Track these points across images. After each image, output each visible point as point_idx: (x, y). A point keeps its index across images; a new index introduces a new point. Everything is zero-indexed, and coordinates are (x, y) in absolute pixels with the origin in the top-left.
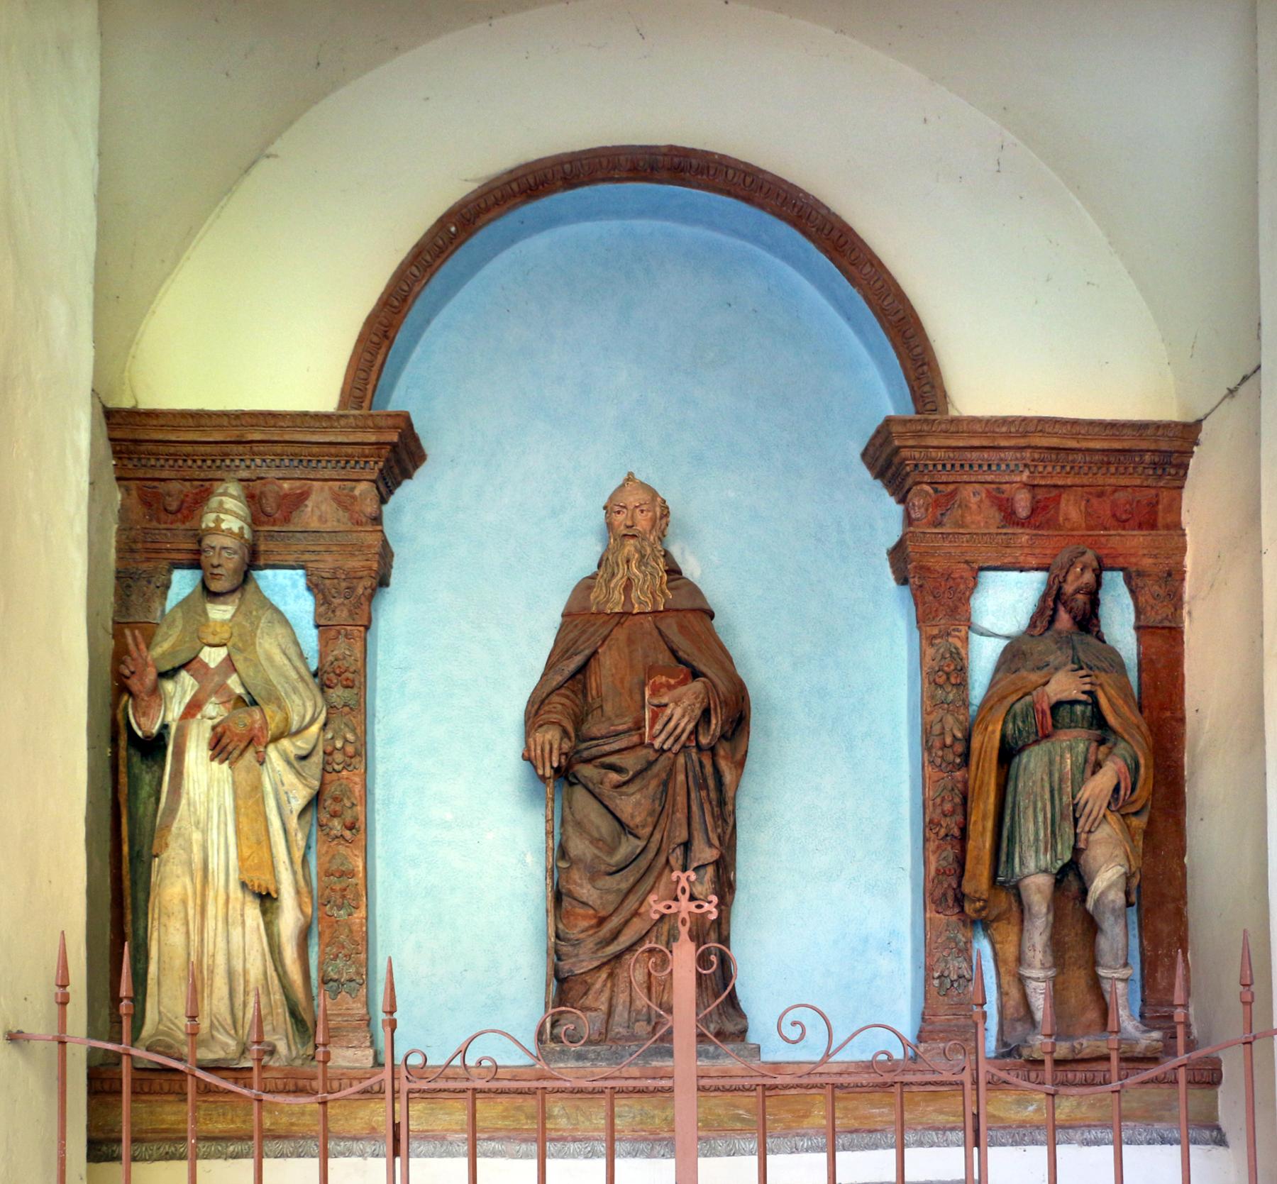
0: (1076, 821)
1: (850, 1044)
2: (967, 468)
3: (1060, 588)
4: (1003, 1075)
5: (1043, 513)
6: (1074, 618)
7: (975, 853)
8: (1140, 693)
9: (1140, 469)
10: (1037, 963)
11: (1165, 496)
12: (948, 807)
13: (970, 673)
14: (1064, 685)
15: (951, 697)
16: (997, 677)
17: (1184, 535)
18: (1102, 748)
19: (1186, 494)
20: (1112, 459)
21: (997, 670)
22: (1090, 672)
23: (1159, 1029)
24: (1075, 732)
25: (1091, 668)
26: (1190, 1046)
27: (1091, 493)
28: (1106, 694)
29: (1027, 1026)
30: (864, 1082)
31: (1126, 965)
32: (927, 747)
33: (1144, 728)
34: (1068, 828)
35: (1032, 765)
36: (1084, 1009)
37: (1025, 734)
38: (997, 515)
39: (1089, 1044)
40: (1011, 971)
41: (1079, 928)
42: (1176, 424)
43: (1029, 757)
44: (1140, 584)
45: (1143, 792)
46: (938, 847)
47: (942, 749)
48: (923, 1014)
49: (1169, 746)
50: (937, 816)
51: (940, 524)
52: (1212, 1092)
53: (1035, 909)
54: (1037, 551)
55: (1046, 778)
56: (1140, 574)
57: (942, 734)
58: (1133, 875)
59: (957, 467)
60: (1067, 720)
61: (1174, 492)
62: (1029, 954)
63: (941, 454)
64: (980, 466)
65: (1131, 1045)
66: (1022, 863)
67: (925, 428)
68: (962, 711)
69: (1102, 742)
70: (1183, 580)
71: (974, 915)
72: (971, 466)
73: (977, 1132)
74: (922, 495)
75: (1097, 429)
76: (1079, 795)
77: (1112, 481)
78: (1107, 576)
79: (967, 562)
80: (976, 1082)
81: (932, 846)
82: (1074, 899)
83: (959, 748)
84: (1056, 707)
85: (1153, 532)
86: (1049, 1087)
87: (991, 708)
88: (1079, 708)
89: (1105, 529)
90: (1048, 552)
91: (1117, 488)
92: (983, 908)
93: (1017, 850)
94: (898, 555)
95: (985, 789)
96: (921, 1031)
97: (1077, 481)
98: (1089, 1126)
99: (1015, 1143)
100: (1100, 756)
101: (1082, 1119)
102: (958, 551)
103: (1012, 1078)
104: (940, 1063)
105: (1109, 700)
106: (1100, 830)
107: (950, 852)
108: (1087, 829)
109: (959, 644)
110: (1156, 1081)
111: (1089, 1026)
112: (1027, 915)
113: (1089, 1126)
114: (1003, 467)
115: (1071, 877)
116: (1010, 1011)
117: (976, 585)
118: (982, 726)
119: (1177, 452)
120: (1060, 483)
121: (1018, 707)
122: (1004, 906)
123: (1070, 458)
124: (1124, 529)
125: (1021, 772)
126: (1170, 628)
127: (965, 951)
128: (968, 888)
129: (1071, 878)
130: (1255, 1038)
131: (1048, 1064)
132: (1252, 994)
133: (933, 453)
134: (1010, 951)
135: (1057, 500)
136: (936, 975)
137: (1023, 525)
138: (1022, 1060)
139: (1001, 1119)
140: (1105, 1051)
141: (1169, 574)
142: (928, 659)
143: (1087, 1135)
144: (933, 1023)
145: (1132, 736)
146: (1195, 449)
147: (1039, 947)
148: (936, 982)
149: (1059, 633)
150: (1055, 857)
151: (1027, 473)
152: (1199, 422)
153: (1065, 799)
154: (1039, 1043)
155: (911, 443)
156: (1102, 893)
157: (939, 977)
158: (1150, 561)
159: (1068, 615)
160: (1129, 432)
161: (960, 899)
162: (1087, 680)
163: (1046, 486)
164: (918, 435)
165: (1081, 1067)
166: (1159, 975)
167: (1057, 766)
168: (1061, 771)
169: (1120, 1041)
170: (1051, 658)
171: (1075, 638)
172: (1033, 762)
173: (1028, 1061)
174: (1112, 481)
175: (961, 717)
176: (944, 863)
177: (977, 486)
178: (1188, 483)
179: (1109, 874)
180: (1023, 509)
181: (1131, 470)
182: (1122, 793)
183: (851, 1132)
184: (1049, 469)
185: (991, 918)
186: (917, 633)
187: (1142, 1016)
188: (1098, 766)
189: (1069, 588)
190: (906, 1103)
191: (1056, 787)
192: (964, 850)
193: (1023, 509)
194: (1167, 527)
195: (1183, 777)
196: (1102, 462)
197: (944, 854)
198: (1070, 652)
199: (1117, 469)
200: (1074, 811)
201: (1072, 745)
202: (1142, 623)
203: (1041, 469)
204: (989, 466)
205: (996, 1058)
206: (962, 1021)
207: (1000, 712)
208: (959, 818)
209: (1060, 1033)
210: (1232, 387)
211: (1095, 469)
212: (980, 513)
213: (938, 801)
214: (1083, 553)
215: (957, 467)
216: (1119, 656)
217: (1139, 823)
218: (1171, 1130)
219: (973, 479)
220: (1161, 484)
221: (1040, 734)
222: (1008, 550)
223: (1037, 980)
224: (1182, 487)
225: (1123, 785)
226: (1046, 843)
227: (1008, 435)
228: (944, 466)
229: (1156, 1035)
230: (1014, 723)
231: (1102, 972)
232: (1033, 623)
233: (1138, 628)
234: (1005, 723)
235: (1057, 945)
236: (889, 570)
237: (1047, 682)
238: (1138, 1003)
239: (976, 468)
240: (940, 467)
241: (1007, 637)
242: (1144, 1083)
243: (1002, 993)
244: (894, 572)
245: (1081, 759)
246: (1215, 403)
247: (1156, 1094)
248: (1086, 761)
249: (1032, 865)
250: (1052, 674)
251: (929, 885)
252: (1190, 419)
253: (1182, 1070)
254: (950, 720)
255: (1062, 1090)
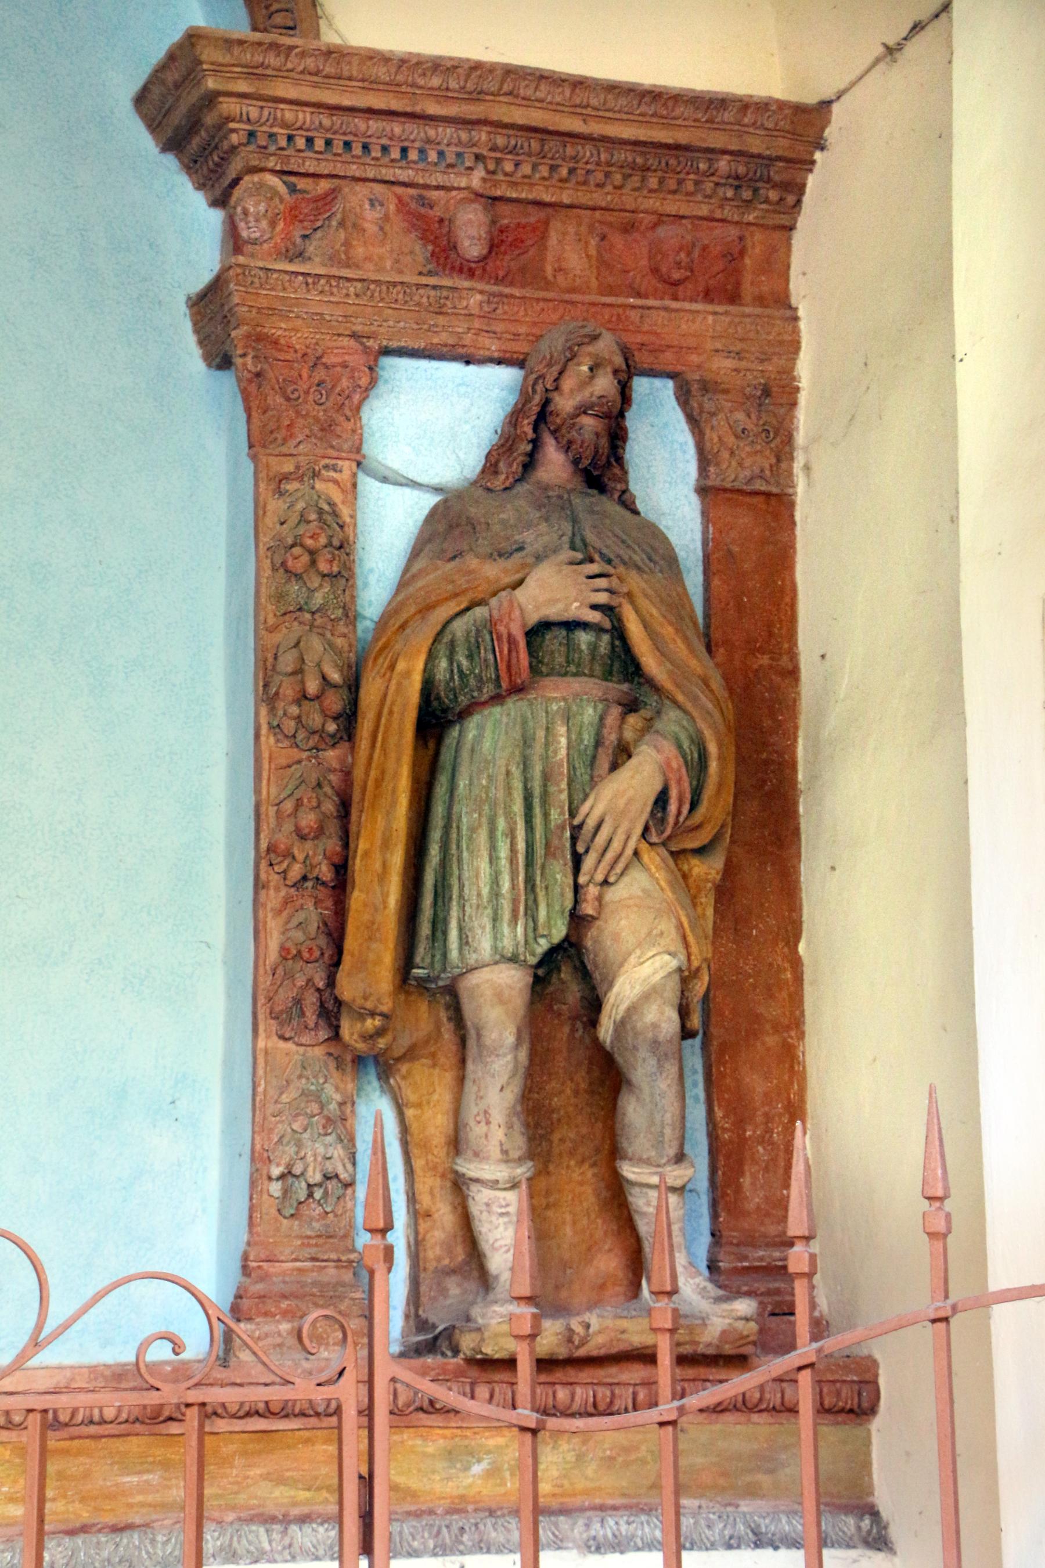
0: (577, 861)
1: (78, 1326)
2: (357, 150)
3: (546, 402)
4: (429, 1388)
5: (511, 251)
6: (576, 462)
7: (366, 917)
8: (707, 616)
9: (708, 186)
10: (495, 1152)
11: (757, 243)
12: (308, 819)
13: (359, 554)
14: (555, 590)
15: (318, 599)
16: (414, 569)
17: (796, 319)
18: (632, 719)
19: (799, 240)
20: (653, 162)
21: (416, 553)
22: (609, 569)
23: (749, 1294)
24: (577, 684)
25: (609, 562)
26: (819, 1328)
27: (610, 225)
28: (637, 611)
29: (472, 1285)
30: (109, 1413)
31: (680, 1158)
32: (267, 695)
33: (717, 682)
34: (560, 874)
35: (487, 744)
36: (590, 1251)
37: (472, 682)
38: (418, 247)
39: (602, 1326)
40: (446, 1159)
41: (582, 1080)
42: (782, 105)
43: (481, 728)
44: (709, 406)
45: (715, 807)
46: (286, 902)
47: (298, 702)
48: (245, 1258)
49: (767, 723)
50: (284, 837)
51: (300, 255)
52: (859, 1431)
53: (491, 1036)
54: (499, 327)
55: (516, 772)
56: (707, 387)
57: (299, 672)
58: (695, 974)
59: (338, 147)
60: (560, 659)
61: (778, 235)
62: (476, 1131)
63: (305, 116)
64: (385, 149)
65: (691, 1329)
66: (464, 941)
67: (272, 60)
68: (342, 628)
69: (631, 706)
70: (794, 404)
71: (361, 1046)
72: (366, 147)
73: (367, 1518)
74: (260, 199)
75: (623, 101)
76: (584, 809)
77: (652, 203)
78: (641, 385)
79: (354, 336)
80: (368, 1412)
81: (273, 898)
82: (574, 1018)
83: (335, 702)
84: (538, 631)
85: (731, 308)
86: (527, 1416)
87: (403, 627)
88: (584, 638)
89: (639, 295)
90: (523, 330)
91: (661, 219)
92: (380, 1032)
93: (454, 913)
94: (211, 310)
95: (387, 786)
96: (238, 1297)
97: (583, 198)
98: (602, 1508)
99: (442, 1550)
100: (629, 735)
101: (586, 1492)
102: (339, 311)
103: (449, 1396)
104: (288, 1362)
105: (646, 626)
106: (626, 879)
107: (312, 914)
108: (599, 877)
109: (337, 496)
110: (743, 1406)
111: (602, 1287)
112: (471, 1043)
113: (602, 1508)
114: (433, 156)
115: (566, 973)
116: (433, 1253)
117: (373, 382)
118: (384, 662)
119: (779, 158)
120: (547, 198)
121: (459, 627)
122: (425, 1026)
123: (569, 151)
124: (675, 298)
125: (465, 754)
126: (768, 495)
127: (339, 1124)
128: (348, 988)
129: (566, 973)
130: (954, 1309)
131: (525, 1367)
132: (948, 1216)
133: (289, 114)
134: (435, 1123)
135: (541, 231)
136: (276, 1171)
137: (471, 273)
138: (459, 1360)
139: (414, 1495)
140: (648, 1339)
141: (767, 392)
142: (270, 520)
143: (596, 1529)
144: (264, 1278)
145: (695, 699)
146: (818, 156)
147: (498, 1116)
148: (276, 1188)
149: (546, 488)
150: (534, 931)
151: (479, 173)
152: (826, 105)
153: (554, 814)
154: (500, 1323)
155: (242, 87)
156: (633, 1010)
157: (282, 1177)
158: (729, 363)
159: (564, 454)
160: (687, 111)
161: (331, 1011)
162: (602, 583)
163: (517, 201)
164: (254, 73)
165: (586, 1375)
166: (746, 1181)
167: (538, 748)
168: (545, 758)
169: (676, 1313)
170: (528, 536)
171: (577, 500)
172: (487, 739)
173: (470, 1361)
174: (652, 203)
175: (339, 642)
176: (299, 936)
177: (378, 188)
178: (802, 222)
179: (647, 969)
180: (471, 232)
181: (690, 186)
182: (673, 808)
183: (72, 1533)
184: (526, 169)
185: (397, 1052)
186: (248, 467)
187: (713, 1267)
188: (623, 753)
189: (565, 403)
190: (209, 1458)
191: (537, 791)
192: (341, 911)
193: (471, 232)
194: (760, 300)
195: (793, 783)
196: (633, 166)
197: (301, 916)
198: (567, 527)
199: (661, 181)
200: (574, 839)
201: (569, 710)
202: (714, 481)
203: (509, 167)
204: (404, 151)
205: (402, 1355)
206: (331, 1272)
207: (422, 636)
208: (332, 844)
209: (545, 1300)
210: (891, 43)
211: (618, 178)
212: (382, 243)
213: (288, 806)
214: (595, 338)
215: (338, 147)
216: (665, 540)
217: (707, 870)
218: (774, 1515)
219: (371, 174)
220: (751, 218)
221: (505, 685)
222: (441, 320)
223: (494, 1184)
224: (791, 228)
225: (674, 793)
226: (515, 902)
227: (443, 95)
228: (310, 141)
229: (745, 1306)
230: (451, 660)
231: (629, 1171)
232: (491, 466)
233: (702, 491)
234: (431, 656)
235: (536, 1117)
236: (190, 340)
237: (520, 583)
238: (706, 1239)
239: (376, 153)
240: (301, 143)
241: (437, 489)
242: (718, 1409)
243: (417, 1214)
244: (201, 343)
245: (588, 739)
246: (858, 72)
247: (743, 1435)
248: (598, 743)
249: (484, 945)
250: (526, 568)
251: (266, 982)
252: (810, 98)
253: (807, 1374)
254: (316, 644)
255: (552, 1423)
